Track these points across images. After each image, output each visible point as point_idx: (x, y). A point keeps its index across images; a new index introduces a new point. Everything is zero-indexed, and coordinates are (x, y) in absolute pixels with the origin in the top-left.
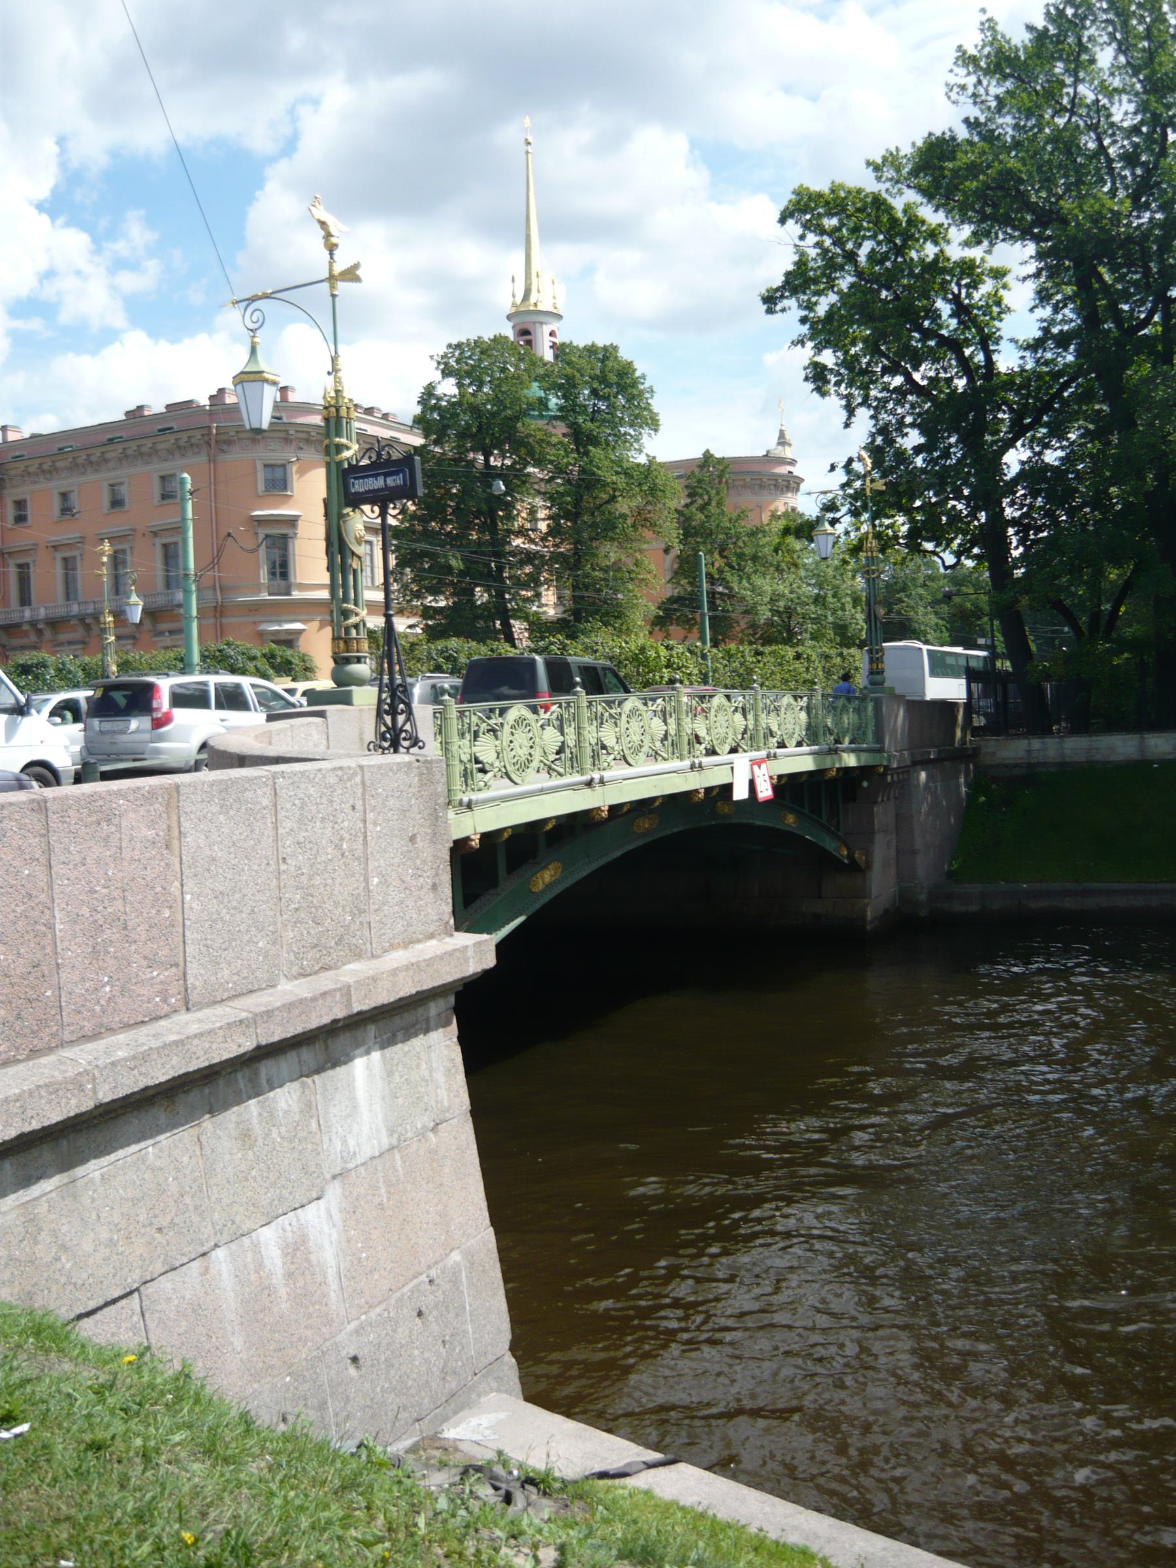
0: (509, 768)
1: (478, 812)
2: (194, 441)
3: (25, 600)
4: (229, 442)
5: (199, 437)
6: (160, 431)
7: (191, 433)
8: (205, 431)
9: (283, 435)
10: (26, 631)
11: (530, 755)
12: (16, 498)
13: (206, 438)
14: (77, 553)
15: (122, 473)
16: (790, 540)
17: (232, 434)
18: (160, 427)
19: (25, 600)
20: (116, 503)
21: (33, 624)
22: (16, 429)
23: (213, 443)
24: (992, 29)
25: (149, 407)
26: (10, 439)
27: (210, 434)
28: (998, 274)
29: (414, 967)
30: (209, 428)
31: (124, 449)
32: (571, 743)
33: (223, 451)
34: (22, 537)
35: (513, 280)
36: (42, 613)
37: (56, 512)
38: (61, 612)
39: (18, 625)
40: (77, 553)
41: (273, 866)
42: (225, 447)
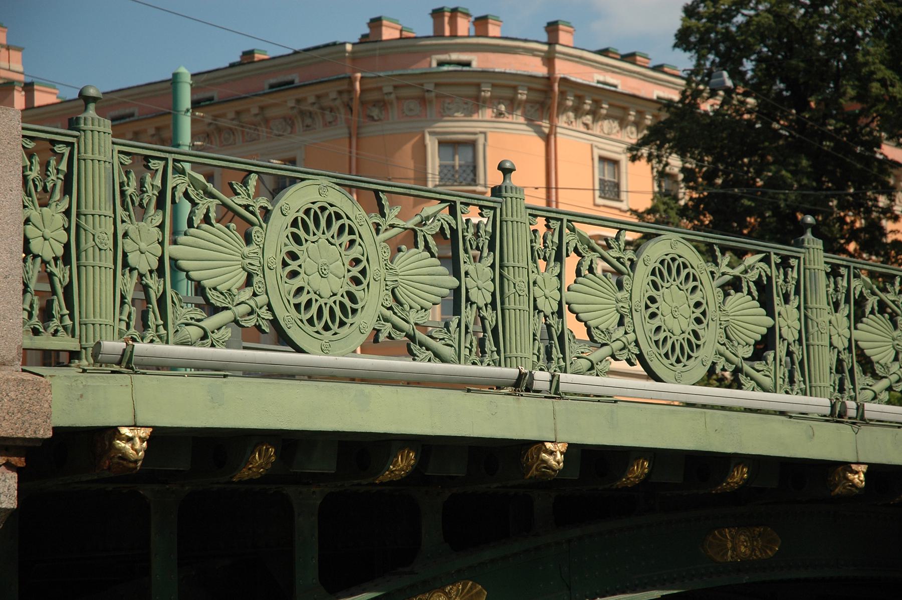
0: (281, 314)
2: (326, 102)
4: (382, 104)
5: (333, 95)
6: (272, 86)
7: (320, 90)
8: (344, 86)
9: (472, 91)
11: (696, 334)
13: (345, 97)
17: (387, 89)
18: (273, 81)
23: (356, 105)
26: (36, 104)
27: (351, 90)
28: (426, 115)
29: (393, 360)
30: (351, 80)
31: (158, 129)
32: (791, 335)
33: (372, 118)
41: (568, 363)
42: (375, 112)
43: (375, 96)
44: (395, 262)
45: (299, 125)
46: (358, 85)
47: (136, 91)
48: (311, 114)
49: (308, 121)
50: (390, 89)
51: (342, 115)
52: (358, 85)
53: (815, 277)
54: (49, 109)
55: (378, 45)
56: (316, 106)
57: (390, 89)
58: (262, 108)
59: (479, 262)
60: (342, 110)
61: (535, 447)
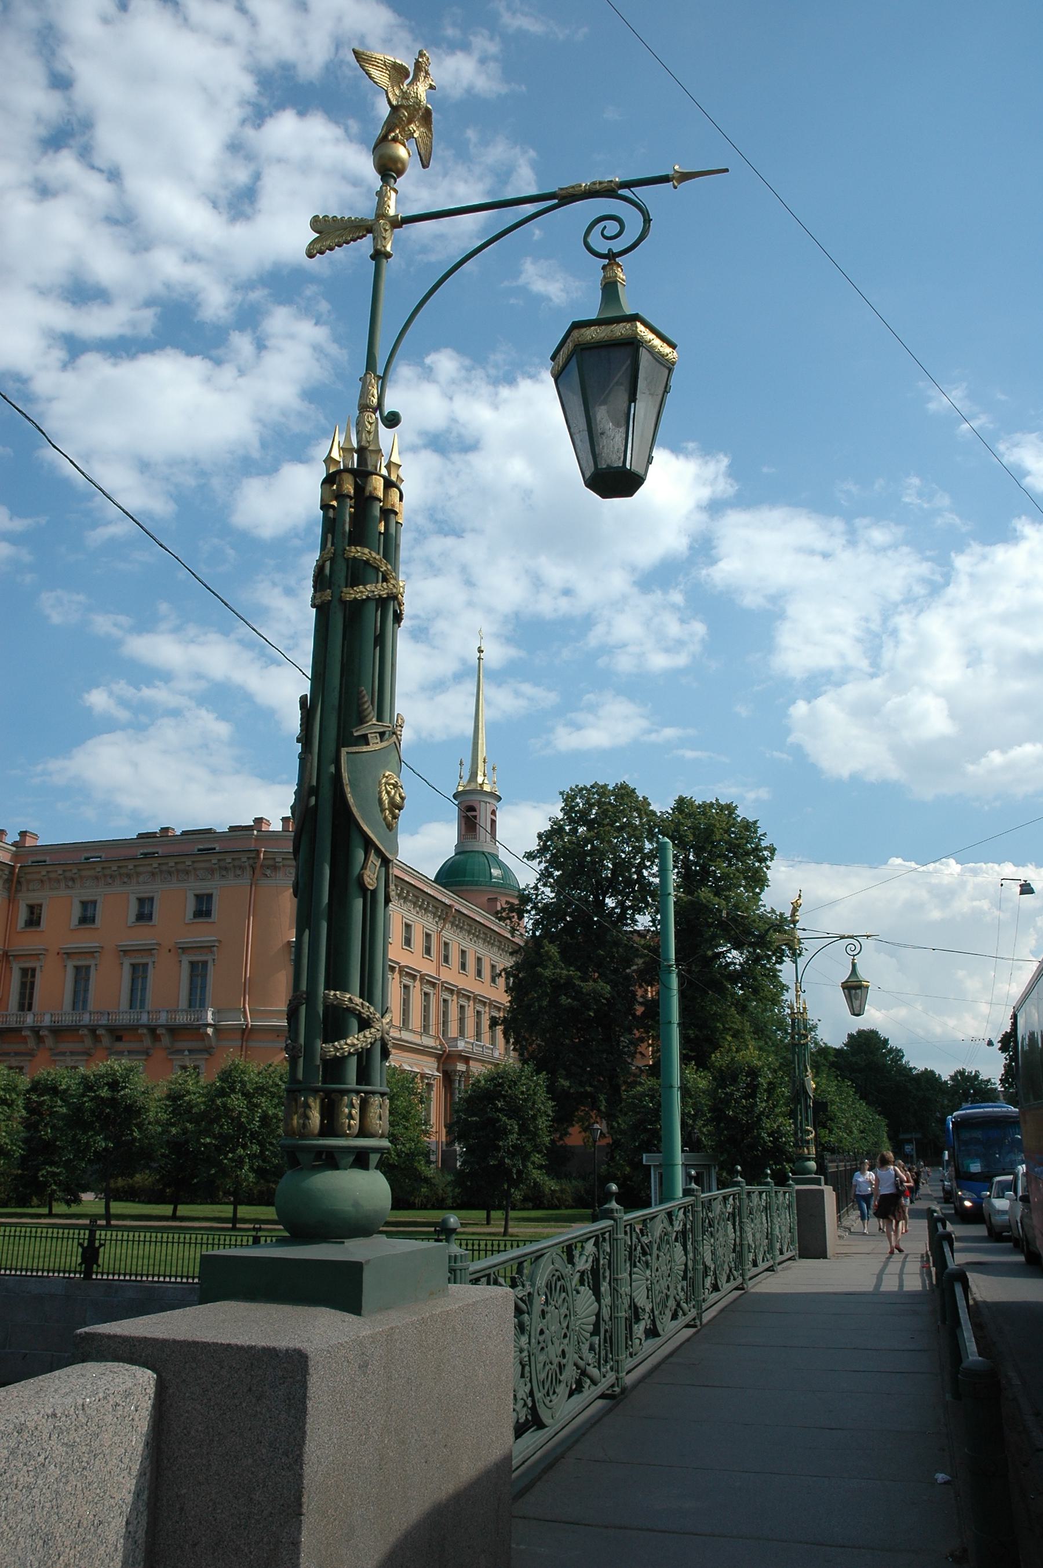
1: (684, 1324)
3: (26, 1003)
6: (199, 850)
10: (25, 1037)
12: (30, 902)
13: (251, 861)
14: (208, 958)
15: (212, 886)
16: (639, 1073)
18: (35, 859)
19: (26, 1003)
20: (87, 919)
21: (36, 1030)
22: (35, 836)
23: (258, 866)
24: (701, 508)
25: (173, 829)
30: (258, 852)
34: (29, 942)
35: (461, 764)
36: (47, 1021)
37: (132, 918)
38: (68, 1020)
39: (17, 1030)
40: (208, 958)
42: (268, 872)
43: (270, 862)
44: (661, 1332)
45: (63, 885)
46: (262, 855)
47: (50, 847)
48: (226, 869)
49: (224, 873)
50: (280, 860)
51: (248, 872)
52: (262, 855)
53: (523, 1463)
54: (120, 842)
55: (22, 849)
56: (216, 866)
57: (280, 860)
58: (135, 866)
59: (922, 1254)
60: (248, 869)
61: (954, 517)
